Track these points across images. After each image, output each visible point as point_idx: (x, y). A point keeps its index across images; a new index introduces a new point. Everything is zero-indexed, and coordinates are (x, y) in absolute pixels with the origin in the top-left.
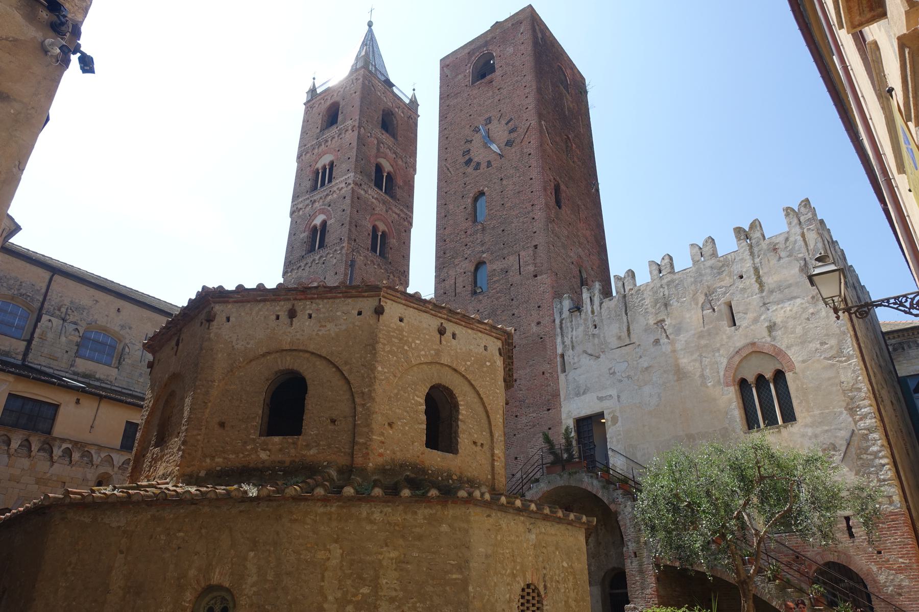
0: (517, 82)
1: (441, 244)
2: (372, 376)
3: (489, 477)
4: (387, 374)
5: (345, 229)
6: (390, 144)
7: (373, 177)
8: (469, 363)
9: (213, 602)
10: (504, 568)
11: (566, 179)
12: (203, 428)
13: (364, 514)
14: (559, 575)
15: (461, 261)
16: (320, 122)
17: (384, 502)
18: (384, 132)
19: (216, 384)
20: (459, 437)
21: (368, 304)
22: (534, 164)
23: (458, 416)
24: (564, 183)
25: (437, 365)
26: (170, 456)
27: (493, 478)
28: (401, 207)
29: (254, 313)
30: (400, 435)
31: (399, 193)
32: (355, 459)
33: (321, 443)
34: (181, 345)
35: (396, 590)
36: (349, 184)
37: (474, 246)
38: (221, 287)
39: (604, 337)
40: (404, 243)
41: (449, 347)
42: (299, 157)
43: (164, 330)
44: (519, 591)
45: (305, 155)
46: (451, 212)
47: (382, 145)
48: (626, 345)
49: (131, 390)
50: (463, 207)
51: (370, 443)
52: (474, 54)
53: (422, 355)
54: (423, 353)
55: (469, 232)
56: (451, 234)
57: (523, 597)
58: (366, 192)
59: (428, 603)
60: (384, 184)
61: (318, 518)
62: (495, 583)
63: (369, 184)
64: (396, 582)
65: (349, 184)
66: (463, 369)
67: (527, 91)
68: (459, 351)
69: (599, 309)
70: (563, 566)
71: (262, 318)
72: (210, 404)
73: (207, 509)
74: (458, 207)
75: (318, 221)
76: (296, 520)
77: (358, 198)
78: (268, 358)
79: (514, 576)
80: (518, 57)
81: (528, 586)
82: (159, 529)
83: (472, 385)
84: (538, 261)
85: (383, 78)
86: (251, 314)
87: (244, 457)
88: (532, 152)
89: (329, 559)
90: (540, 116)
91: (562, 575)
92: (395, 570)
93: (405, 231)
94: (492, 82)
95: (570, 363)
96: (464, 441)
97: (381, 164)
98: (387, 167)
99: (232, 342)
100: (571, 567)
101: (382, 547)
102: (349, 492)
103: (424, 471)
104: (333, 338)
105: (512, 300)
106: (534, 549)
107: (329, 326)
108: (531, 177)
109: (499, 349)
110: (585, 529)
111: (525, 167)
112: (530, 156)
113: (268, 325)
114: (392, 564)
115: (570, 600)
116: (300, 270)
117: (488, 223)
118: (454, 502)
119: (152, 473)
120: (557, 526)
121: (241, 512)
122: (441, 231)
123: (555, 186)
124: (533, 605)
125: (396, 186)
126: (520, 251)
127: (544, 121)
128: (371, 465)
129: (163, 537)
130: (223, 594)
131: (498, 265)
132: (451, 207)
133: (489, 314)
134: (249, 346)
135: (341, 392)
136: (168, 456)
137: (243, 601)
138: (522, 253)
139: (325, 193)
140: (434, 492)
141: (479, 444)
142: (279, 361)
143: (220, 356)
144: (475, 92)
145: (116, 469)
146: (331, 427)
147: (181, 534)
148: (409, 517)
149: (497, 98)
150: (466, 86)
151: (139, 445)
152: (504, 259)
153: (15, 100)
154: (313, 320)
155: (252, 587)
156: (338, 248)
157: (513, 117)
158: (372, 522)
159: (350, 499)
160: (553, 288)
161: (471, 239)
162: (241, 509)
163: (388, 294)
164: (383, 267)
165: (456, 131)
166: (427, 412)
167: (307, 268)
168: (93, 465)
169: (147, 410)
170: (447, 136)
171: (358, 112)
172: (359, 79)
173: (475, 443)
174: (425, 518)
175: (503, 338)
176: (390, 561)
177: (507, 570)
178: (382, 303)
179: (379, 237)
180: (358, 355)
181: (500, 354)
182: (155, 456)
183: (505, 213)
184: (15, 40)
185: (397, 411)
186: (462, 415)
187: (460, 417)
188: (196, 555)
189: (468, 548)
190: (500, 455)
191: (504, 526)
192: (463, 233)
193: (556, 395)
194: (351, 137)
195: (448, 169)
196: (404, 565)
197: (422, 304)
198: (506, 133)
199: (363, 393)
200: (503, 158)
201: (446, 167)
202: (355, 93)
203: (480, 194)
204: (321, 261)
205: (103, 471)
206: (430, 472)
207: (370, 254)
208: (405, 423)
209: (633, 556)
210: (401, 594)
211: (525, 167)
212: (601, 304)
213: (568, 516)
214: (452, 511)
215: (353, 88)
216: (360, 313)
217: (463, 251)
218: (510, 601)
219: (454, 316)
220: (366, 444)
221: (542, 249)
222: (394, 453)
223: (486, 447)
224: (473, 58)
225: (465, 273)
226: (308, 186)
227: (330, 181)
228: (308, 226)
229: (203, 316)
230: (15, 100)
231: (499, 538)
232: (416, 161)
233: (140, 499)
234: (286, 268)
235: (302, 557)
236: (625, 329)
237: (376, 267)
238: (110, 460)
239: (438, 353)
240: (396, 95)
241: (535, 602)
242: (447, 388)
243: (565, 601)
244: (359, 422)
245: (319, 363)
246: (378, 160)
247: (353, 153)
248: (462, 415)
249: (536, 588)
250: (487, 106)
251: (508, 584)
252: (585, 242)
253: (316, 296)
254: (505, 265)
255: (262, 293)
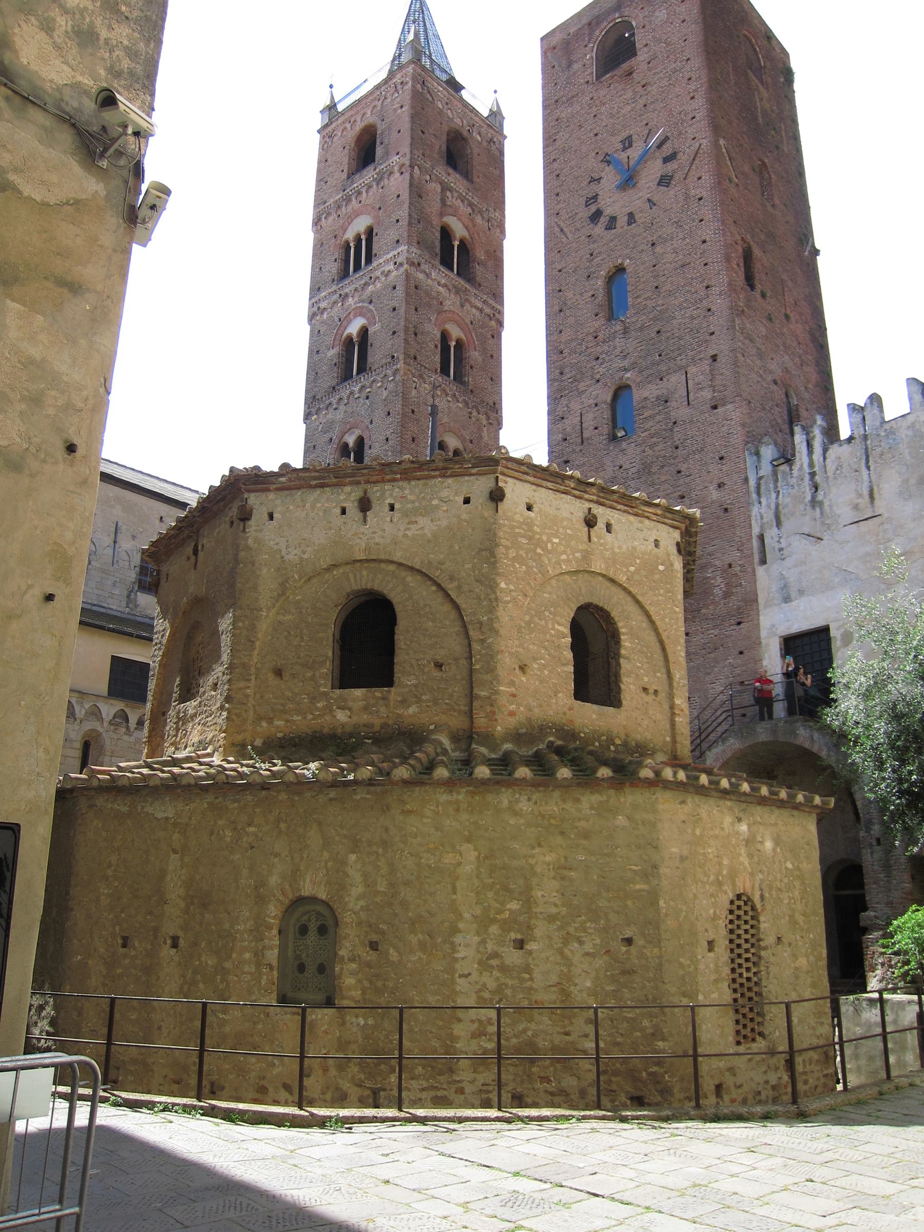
0: (675, 71)
1: (555, 358)
2: (493, 596)
3: (668, 739)
4: (514, 594)
5: (399, 340)
6: (462, 190)
7: (438, 250)
8: (632, 569)
9: (306, 918)
10: (706, 874)
11: (763, 237)
12: (253, 677)
13: (506, 803)
14: (781, 881)
15: (589, 386)
16: (346, 160)
17: (533, 786)
18: (451, 171)
19: (264, 614)
20: (621, 681)
21: (480, 486)
22: (709, 216)
23: (619, 649)
24: (758, 244)
25: (586, 575)
26: (207, 717)
27: (674, 741)
28: (485, 297)
29: (308, 505)
30: (537, 683)
31: (479, 271)
32: (475, 721)
33: (424, 697)
34: (201, 554)
35: (556, 905)
36: (401, 264)
37: (610, 360)
38: (257, 468)
39: (831, 506)
40: (492, 356)
41: (601, 545)
42: (317, 222)
43: (172, 532)
44: (727, 905)
45: (326, 218)
46: (569, 303)
47: (448, 194)
48: (866, 519)
49: (104, 607)
50: (590, 294)
51: (497, 696)
52: (598, 24)
53: (564, 561)
54: (564, 557)
55: (601, 337)
56: (572, 340)
57: (731, 912)
58: (428, 275)
59: (602, 922)
60: (455, 260)
61: (440, 809)
62: (695, 895)
63: (433, 261)
64: (555, 894)
65: (401, 264)
66: (624, 579)
67: (692, 87)
68: (617, 550)
69: (822, 459)
70: (786, 868)
71: (321, 514)
72: (258, 643)
73: (283, 796)
74: (581, 294)
75: (353, 329)
76: (410, 812)
77: (416, 287)
78: (335, 572)
79: (720, 884)
80: (676, 27)
81: (739, 897)
82: (220, 822)
83: (638, 602)
84: (717, 382)
85: (444, 77)
86: (304, 506)
87: (312, 719)
88: (704, 194)
89: (459, 864)
90: (716, 128)
91: (786, 880)
92: (554, 878)
93: (493, 337)
94: (631, 74)
95: (774, 548)
96: (629, 687)
97: (449, 226)
98: (459, 230)
99: (280, 551)
100: (798, 868)
101: (533, 848)
102: (483, 773)
103: (572, 735)
104: (429, 541)
105: (677, 448)
106: (746, 846)
107: (422, 521)
108: (703, 238)
109: (678, 544)
110: (817, 815)
111: (694, 221)
112: (701, 202)
113: (330, 522)
114: (549, 870)
115: (797, 915)
116: (331, 410)
117: (634, 320)
118: (633, 785)
119: (181, 739)
120: (777, 812)
121: (331, 800)
122: (555, 337)
123: (744, 250)
124: (746, 922)
125: (474, 261)
126: (688, 366)
127: (724, 138)
128: (499, 728)
129: (228, 833)
130: (320, 908)
131: (651, 391)
132: (570, 295)
133: (638, 472)
134: (305, 556)
135: (447, 622)
136: (204, 716)
137: (347, 918)
138: (692, 370)
139: (363, 282)
140: (604, 772)
141: (651, 691)
142: (351, 576)
143: (265, 572)
144: (602, 93)
145: (106, 724)
146: (436, 674)
147: (252, 829)
148: (568, 806)
149: (642, 102)
150: (587, 82)
151: (154, 699)
152: (661, 379)
153: (88, 290)
154: (397, 515)
155: (357, 899)
156: (389, 372)
157: (669, 134)
158: (516, 814)
159: (484, 782)
160: (743, 425)
161: (606, 348)
162: (332, 795)
163: (508, 468)
164: (460, 400)
165: (573, 163)
166: (573, 647)
167: (342, 407)
168: (75, 719)
169: (160, 649)
170: (558, 172)
171: (408, 141)
172: (407, 83)
173: (645, 690)
174: (592, 808)
175: (683, 526)
176: (545, 867)
177: (709, 877)
178: (500, 484)
179: (452, 349)
180: (470, 566)
181: (679, 551)
182: (182, 715)
183: (660, 302)
184: (77, 202)
185: (531, 647)
186: (626, 649)
187: (623, 652)
188: (276, 856)
189: (656, 848)
190: (683, 706)
191: (704, 815)
192: (590, 338)
193: (751, 601)
194: (398, 184)
195: (562, 230)
196: (566, 872)
197: (559, 481)
198: (659, 162)
199: (481, 623)
200: (654, 208)
201: (559, 226)
202: (402, 107)
203: (617, 271)
204: (364, 395)
205: (90, 728)
206: (582, 735)
207: (440, 379)
208: (544, 665)
209: (874, 843)
210: (564, 910)
211: (694, 221)
212: (825, 450)
213: (794, 796)
214: (631, 797)
215: (398, 100)
216: (467, 501)
217: (592, 368)
218: (715, 918)
219: (608, 496)
220: (489, 698)
221: (724, 361)
222: (530, 710)
223: (662, 696)
224: (598, 32)
225: (596, 405)
226: (334, 270)
227: (369, 261)
228: (338, 337)
229: (234, 511)
230: (88, 290)
231: (698, 832)
232: (504, 216)
233: (192, 782)
234: (309, 408)
235: (423, 861)
236: (866, 493)
237: (449, 399)
238: (95, 713)
239: (586, 555)
240: (466, 105)
241: (748, 918)
242: (602, 609)
243: (790, 916)
244: (477, 667)
245: (411, 580)
246: (445, 219)
247: (403, 213)
248: (626, 649)
249: (749, 899)
250: (624, 116)
251: (712, 895)
252: (795, 344)
253: (398, 476)
254: (665, 391)
255: (317, 474)
